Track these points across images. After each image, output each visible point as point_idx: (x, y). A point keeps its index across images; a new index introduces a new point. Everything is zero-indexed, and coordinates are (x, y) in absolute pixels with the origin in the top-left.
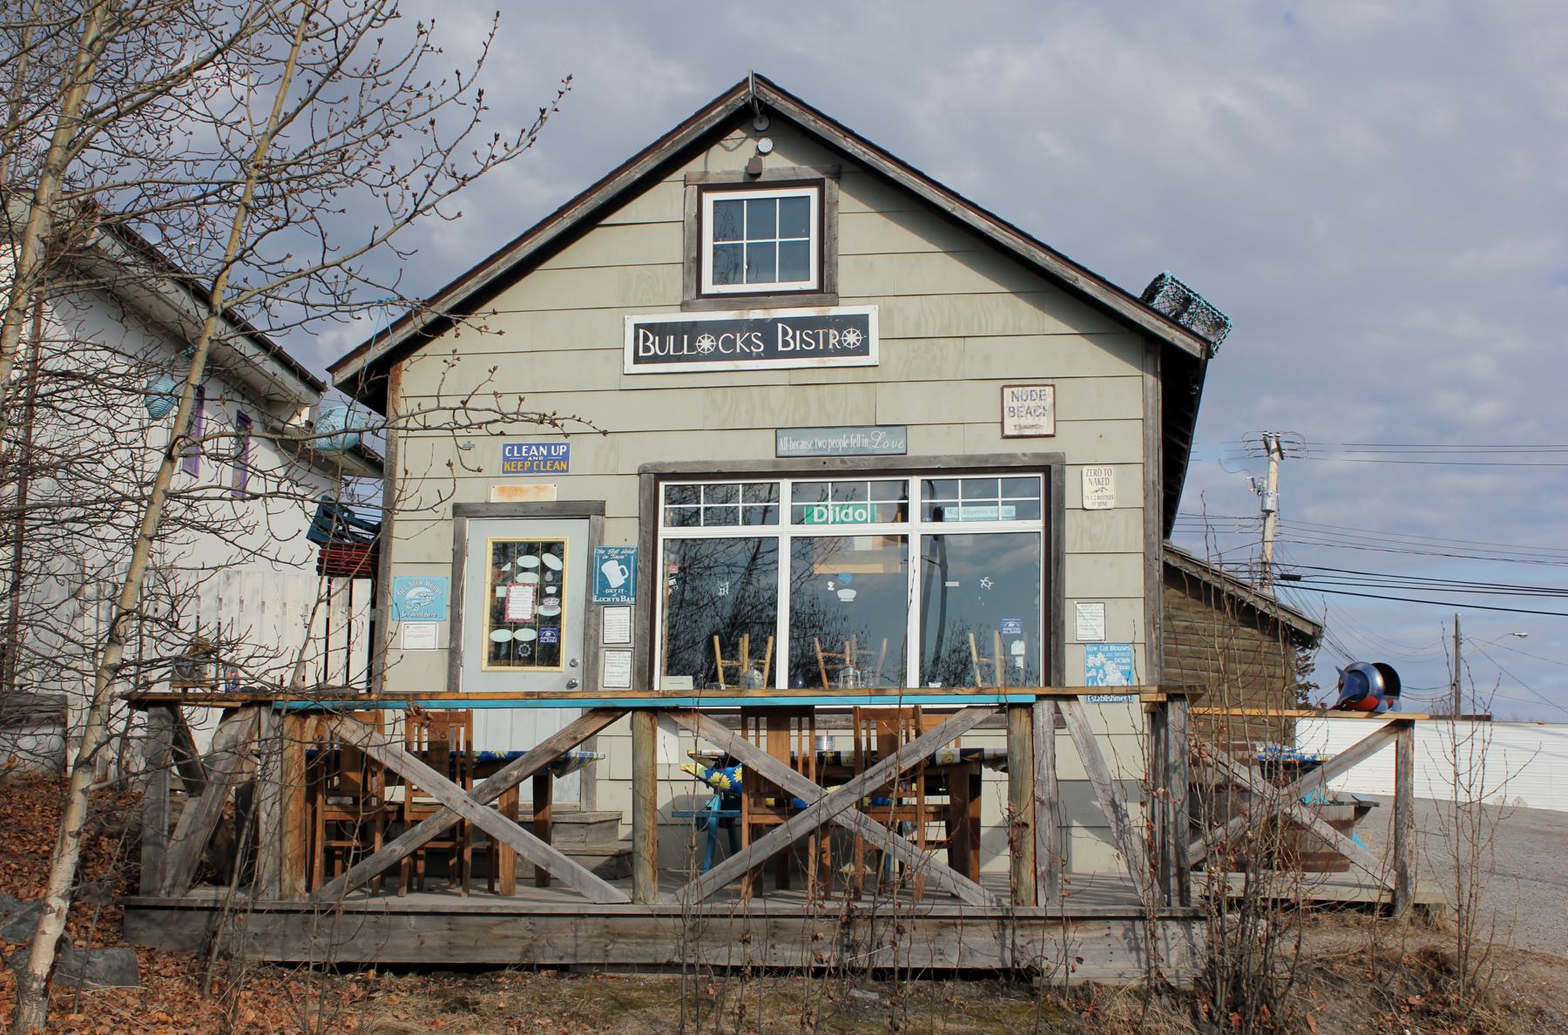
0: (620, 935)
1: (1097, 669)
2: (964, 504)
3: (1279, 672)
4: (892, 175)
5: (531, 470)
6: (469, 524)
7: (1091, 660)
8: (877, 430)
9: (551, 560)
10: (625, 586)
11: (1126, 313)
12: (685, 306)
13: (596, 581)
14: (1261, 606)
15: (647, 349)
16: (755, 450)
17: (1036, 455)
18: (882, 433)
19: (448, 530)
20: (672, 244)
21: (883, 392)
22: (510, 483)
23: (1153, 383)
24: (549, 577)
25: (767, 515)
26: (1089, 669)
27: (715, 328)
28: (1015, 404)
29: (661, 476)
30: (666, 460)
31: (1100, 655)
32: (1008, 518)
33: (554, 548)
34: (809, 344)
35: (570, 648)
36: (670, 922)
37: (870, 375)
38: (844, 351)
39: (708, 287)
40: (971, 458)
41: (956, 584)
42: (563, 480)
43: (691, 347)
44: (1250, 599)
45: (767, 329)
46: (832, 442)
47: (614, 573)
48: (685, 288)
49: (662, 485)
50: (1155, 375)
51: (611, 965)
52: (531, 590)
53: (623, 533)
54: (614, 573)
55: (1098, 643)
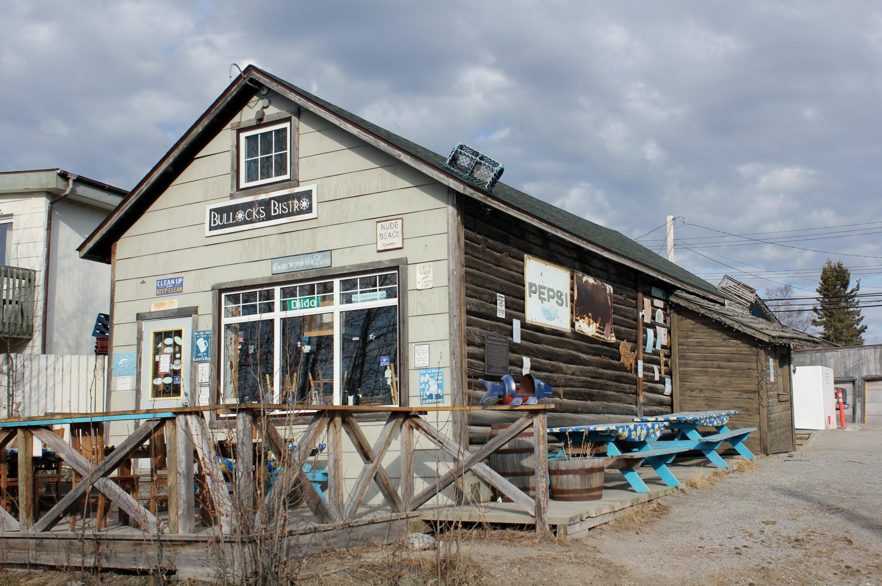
0: (12, 548)
1: (425, 383)
2: (362, 292)
3: (754, 365)
4: (312, 110)
5: (167, 293)
6: (144, 324)
7: (423, 379)
8: (317, 255)
9: (177, 339)
10: (206, 352)
11: (424, 171)
12: (232, 196)
13: (195, 350)
14: (736, 326)
15: (215, 222)
16: (260, 272)
17: (392, 260)
18: (320, 255)
19: (134, 327)
20: (225, 163)
21: (320, 233)
22: (160, 300)
23: (451, 210)
24: (177, 349)
25: (270, 308)
26: (421, 384)
27: (244, 207)
28: (383, 232)
29: (221, 291)
30: (223, 281)
31: (427, 376)
32: (382, 298)
33: (179, 333)
34: (285, 210)
35: (185, 387)
36: (31, 541)
37: (314, 224)
38: (300, 212)
39: (243, 184)
40: (360, 265)
41: (354, 339)
42: (180, 297)
43: (234, 219)
44: (729, 322)
45: (266, 203)
46: (297, 264)
47: (202, 345)
48: (232, 187)
49: (223, 295)
50: (453, 205)
51: (8, 564)
52: (169, 356)
53: (206, 323)
54: (202, 345)
55: (426, 368)
